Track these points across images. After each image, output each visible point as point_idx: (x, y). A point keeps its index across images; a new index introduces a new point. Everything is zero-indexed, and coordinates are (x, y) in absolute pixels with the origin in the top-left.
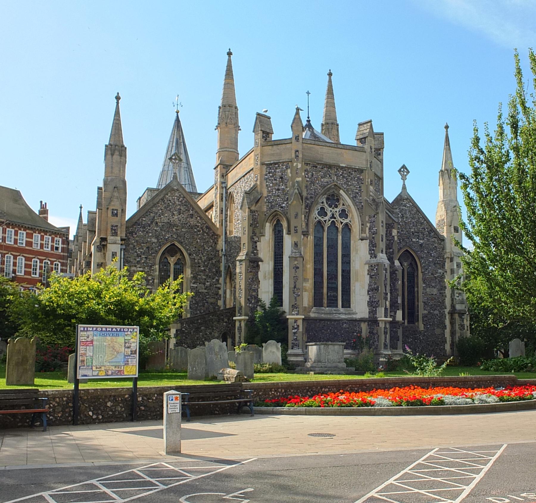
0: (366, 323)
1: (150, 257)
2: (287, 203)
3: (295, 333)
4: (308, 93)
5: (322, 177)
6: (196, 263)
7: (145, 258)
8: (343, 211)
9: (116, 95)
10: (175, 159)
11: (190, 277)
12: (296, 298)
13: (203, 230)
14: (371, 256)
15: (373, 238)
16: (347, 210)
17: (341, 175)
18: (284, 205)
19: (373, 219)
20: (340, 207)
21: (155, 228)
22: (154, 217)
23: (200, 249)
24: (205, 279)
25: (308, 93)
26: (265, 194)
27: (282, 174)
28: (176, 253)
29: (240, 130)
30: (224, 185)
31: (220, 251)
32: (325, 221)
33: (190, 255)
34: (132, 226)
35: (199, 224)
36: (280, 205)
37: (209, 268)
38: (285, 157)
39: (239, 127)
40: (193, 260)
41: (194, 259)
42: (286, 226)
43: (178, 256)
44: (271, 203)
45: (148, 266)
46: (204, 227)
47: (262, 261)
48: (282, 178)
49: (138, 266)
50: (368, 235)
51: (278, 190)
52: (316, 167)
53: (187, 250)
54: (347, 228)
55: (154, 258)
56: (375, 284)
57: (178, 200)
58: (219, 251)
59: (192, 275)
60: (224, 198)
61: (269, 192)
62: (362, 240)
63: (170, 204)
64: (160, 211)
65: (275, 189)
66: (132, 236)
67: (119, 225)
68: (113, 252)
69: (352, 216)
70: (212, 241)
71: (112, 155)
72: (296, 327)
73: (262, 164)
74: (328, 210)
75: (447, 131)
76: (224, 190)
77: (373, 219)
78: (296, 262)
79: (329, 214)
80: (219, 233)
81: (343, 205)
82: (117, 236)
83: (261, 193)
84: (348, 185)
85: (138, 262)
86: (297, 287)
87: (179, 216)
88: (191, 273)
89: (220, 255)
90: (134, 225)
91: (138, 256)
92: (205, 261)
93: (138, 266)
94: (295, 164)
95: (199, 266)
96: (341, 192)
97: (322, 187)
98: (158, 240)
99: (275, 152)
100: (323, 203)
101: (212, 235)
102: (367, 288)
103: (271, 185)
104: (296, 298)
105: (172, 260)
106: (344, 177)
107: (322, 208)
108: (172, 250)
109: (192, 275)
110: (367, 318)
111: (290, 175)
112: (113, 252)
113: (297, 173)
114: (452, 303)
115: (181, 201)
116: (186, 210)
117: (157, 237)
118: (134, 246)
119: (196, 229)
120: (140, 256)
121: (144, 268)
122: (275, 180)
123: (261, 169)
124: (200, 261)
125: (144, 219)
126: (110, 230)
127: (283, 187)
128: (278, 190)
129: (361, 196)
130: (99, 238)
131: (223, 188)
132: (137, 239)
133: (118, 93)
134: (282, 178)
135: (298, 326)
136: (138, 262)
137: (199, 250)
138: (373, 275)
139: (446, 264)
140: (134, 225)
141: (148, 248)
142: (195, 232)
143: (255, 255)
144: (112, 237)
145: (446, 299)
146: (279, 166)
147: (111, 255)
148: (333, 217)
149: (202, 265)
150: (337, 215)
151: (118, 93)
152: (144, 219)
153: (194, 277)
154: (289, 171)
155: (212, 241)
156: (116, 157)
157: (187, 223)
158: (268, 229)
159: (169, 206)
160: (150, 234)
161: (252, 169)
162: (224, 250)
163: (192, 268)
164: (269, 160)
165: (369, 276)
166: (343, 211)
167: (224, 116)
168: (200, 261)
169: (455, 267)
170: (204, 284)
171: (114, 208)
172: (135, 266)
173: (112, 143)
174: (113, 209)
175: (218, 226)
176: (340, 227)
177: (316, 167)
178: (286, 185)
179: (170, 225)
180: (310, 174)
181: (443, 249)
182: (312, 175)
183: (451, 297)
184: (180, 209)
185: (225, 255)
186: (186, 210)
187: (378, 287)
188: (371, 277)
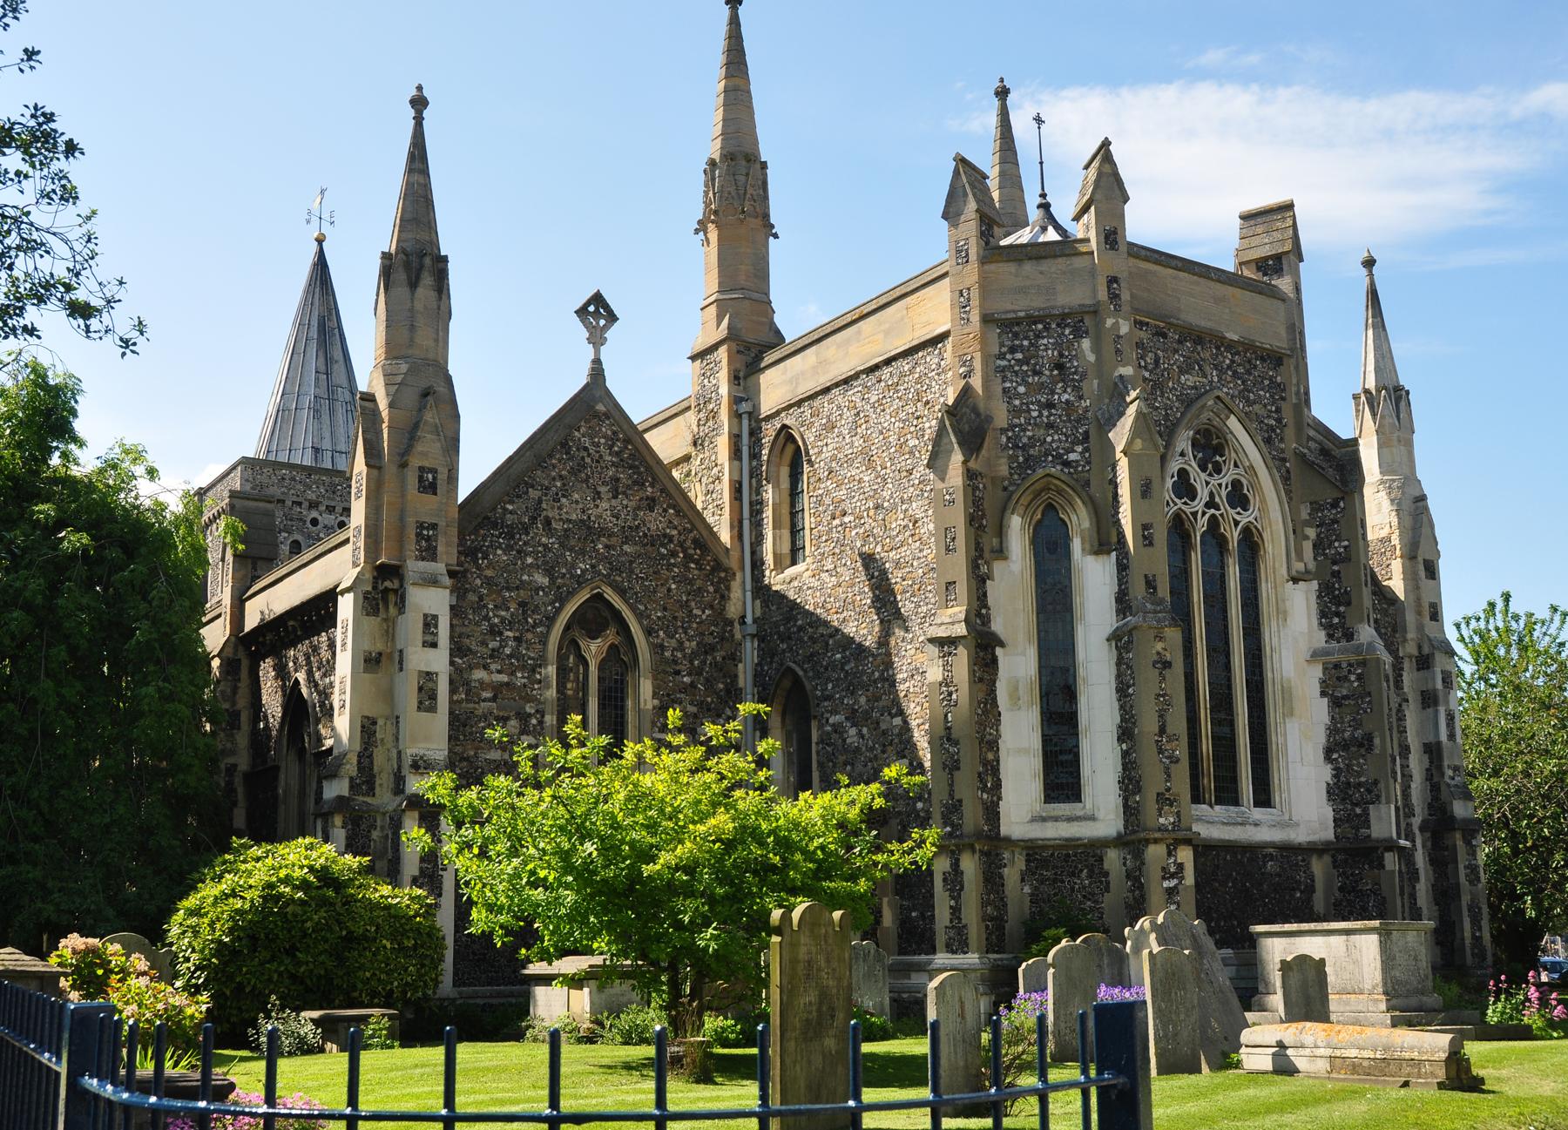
0: (1327, 858)
1: (529, 636)
2: (1086, 450)
3: (1171, 892)
5: (1182, 372)
6: (666, 661)
7: (516, 639)
8: (1236, 484)
9: (414, 92)
10: (596, 314)
11: (649, 706)
13: (685, 551)
15: (1336, 574)
18: (1072, 457)
19: (1330, 514)
20: (1227, 478)
22: (540, 501)
26: (1001, 417)
27: (1061, 355)
28: (604, 627)
29: (776, 236)
30: (745, 407)
31: (737, 625)
32: (1195, 514)
33: (649, 632)
35: (674, 532)
36: (1060, 456)
37: (707, 680)
38: (1071, 296)
39: (772, 226)
40: (658, 649)
41: (662, 647)
42: (1086, 524)
43: (611, 636)
45: (523, 668)
46: (689, 543)
47: (1002, 645)
48: (1060, 366)
49: (493, 667)
50: (1312, 566)
51: (1050, 405)
52: (1164, 336)
53: (640, 616)
54: (1251, 544)
55: (544, 640)
56: (1357, 724)
57: (611, 448)
58: (731, 623)
60: (745, 450)
61: (1015, 412)
62: (1295, 580)
63: (588, 460)
66: (475, 560)
67: (442, 523)
68: (426, 616)
69: (1263, 501)
70: (711, 589)
71: (413, 284)
73: (987, 319)
74: (1198, 478)
75: (1371, 275)
76: (745, 422)
77: (1330, 514)
78: (1159, 646)
79: (1203, 494)
80: (733, 563)
82: (434, 558)
83: (989, 419)
84: (1248, 400)
85: (495, 654)
86: (1169, 730)
87: (614, 502)
88: (655, 695)
89: (738, 636)
91: (494, 632)
92: (694, 654)
93: (493, 667)
94: (1109, 322)
95: (678, 673)
96: (1233, 422)
97: (1182, 402)
98: (552, 579)
99: (1028, 283)
100: (1182, 454)
101: (713, 569)
102: (1321, 738)
103: (1022, 389)
105: (593, 648)
106: (1235, 375)
107: (1183, 473)
108: (596, 617)
109: (656, 702)
110: (1328, 843)
111: (1092, 358)
112: (426, 616)
113: (1118, 351)
115: (618, 454)
116: (635, 483)
117: (549, 572)
118: (481, 598)
120: (501, 634)
121: (513, 673)
122: (1036, 373)
123: (983, 341)
124: (679, 655)
125: (510, 507)
126: (413, 536)
127: (1065, 397)
129: (1282, 440)
130: (369, 567)
131: (739, 416)
132: (489, 573)
133: (420, 88)
134: (1060, 366)
135: (1180, 867)
136: (495, 654)
137: (675, 618)
138: (1345, 697)
141: (522, 604)
142: (663, 557)
143: (983, 624)
144: (421, 564)
146: (1046, 328)
147: (421, 625)
148: (1211, 504)
150: (1222, 497)
151: (420, 88)
152: (510, 507)
154: (1086, 344)
155: (711, 589)
156: (425, 291)
157: (638, 527)
158: (1018, 533)
159: (582, 466)
160: (529, 560)
161: (942, 337)
162: (749, 620)
163: (655, 678)
166: (1236, 484)
167: (732, 189)
168: (679, 655)
169: (1439, 685)
171: (427, 464)
172: (486, 667)
173: (408, 246)
174: (421, 469)
175: (725, 536)
176: (1233, 536)
177: (1164, 336)
178: (1077, 389)
179: (588, 530)
180: (1150, 358)
182: (1157, 362)
184: (618, 480)
185: (753, 636)
186: (635, 483)
187: (1369, 738)
188: (1336, 703)
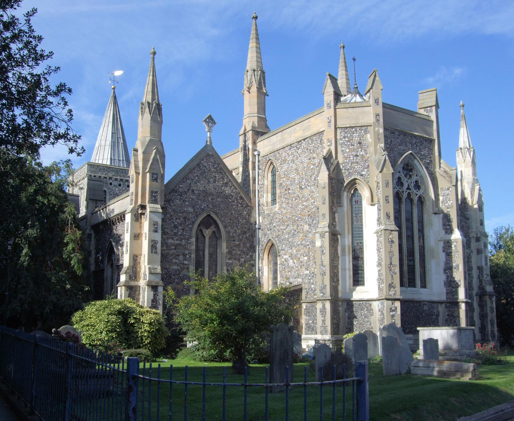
1: (187, 228)
4: (354, 59)
12: (392, 277)
13: (237, 201)
14: (446, 232)
16: (419, 181)
17: (415, 143)
18: (363, 173)
21: (192, 197)
22: (190, 184)
23: (235, 221)
24: (240, 255)
25: (354, 59)
33: (225, 227)
34: (170, 193)
37: (244, 243)
41: (229, 232)
43: (213, 228)
44: (348, 170)
45: (184, 239)
52: (394, 133)
53: (222, 222)
55: (191, 230)
59: (227, 250)
61: (346, 158)
62: (435, 214)
63: (206, 170)
64: (196, 178)
65: (352, 155)
72: (393, 309)
79: (406, 186)
81: (417, 176)
88: (227, 248)
90: (171, 192)
91: (176, 227)
93: (175, 238)
95: (234, 241)
98: (194, 210)
103: (347, 150)
104: (392, 277)
108: (209, 221)
109: (227, 250)
114: (481, 285)
115: (216, 168)
117: (193, 207)
118: (171, 216)
119: (230, 199)
120: (177, 227)
125: (181, 186)
127: (361, 153)
128: (357, 156)
132: (174, 208)
134: (360, 143)
139: (472, 244)
140: (171, 192)
141: (185, 218)
145: (474, 280)
148: (408, 188)
149: (236, 239)
152: (181, 186)
153: (230, 252)
160: (187, 203)
163: (227, 243)
164: (344, 123)
165: (444, 253)
170: (239, 260)
176: (415, 199)
181: (469, 229)
182: (391, 142)
183: (479, 278)
184: (216, 177)
